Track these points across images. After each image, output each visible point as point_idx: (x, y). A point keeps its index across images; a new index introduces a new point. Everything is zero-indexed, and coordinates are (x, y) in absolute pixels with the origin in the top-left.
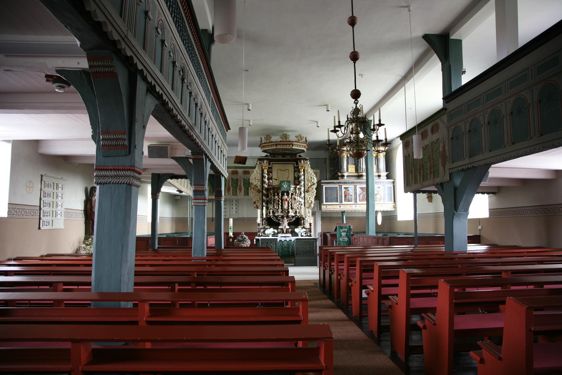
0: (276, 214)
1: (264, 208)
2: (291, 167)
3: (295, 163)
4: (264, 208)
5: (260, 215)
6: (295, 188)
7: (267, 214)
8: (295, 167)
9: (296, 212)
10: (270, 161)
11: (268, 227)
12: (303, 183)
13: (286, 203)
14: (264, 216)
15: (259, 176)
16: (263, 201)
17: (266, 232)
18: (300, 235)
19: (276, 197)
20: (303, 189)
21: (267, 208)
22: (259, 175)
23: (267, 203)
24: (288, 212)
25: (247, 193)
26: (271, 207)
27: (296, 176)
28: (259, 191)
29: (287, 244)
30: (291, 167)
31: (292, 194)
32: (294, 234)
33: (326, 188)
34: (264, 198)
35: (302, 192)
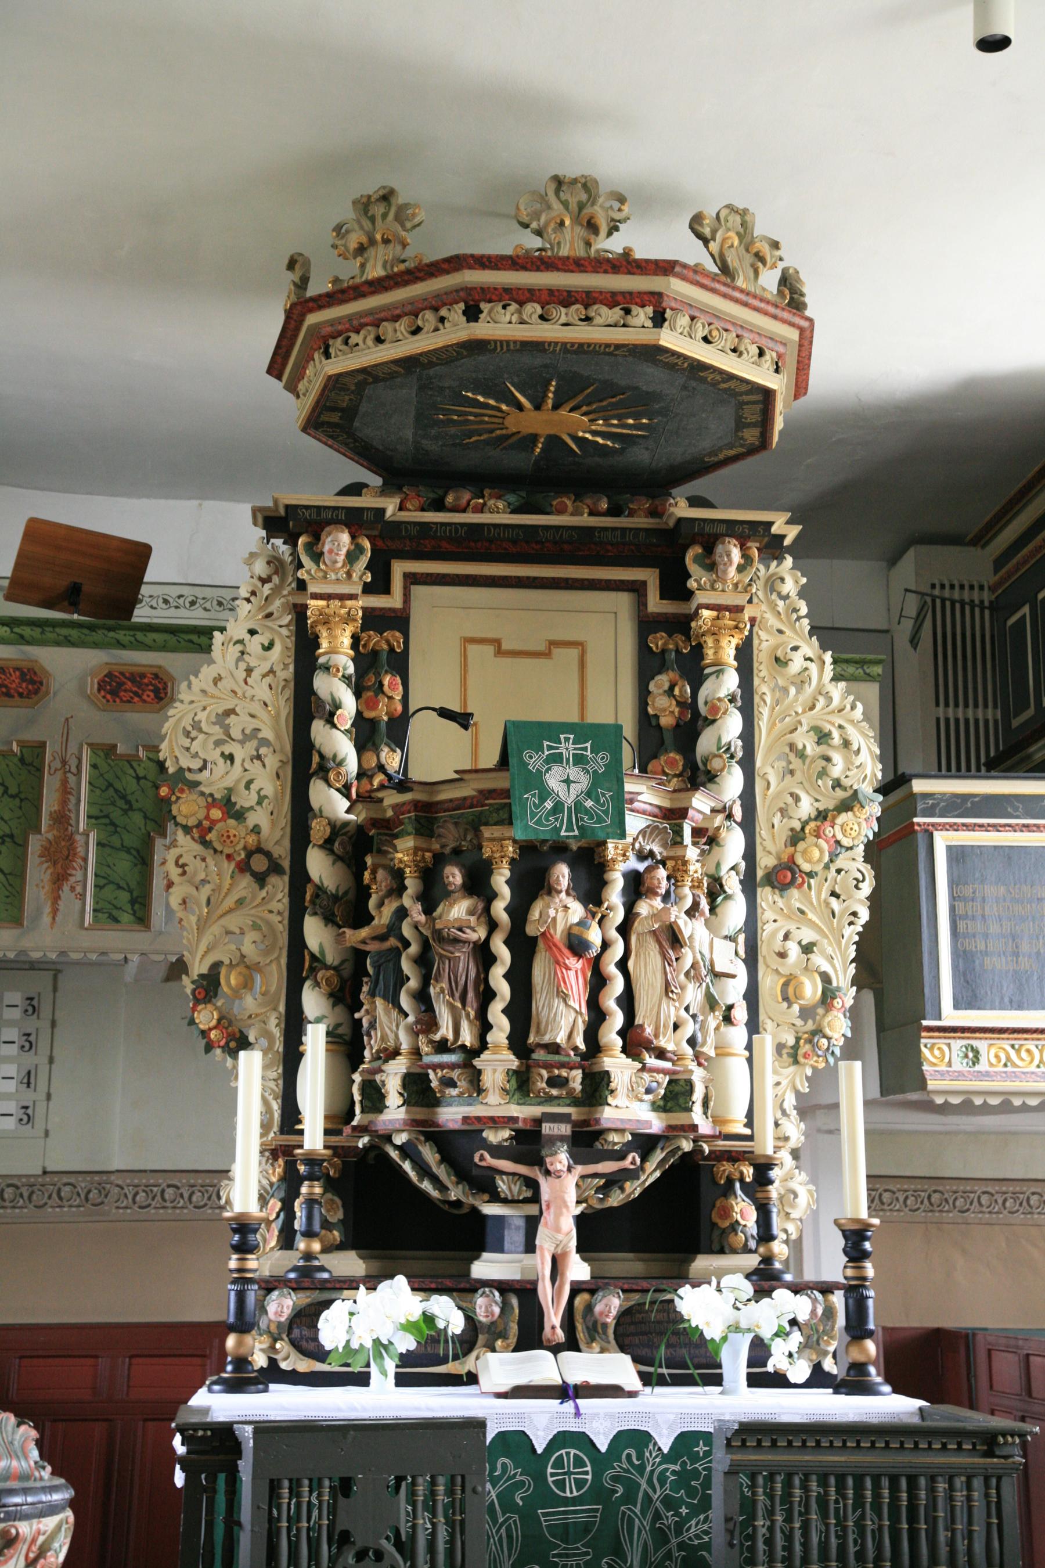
0: (451, 1115)
1: (315, 1041)
2: (603, 625)
3: (650, 576)
4: (315, 1041)
5: (248, 1124)
6: (674, 815)
7: (339, 1119)
8: (646, 625)
9: (676, 1096)
10: (387, 546)
11: (349, 1264)
12: (733, 783)
13: (575, 977)
14: (313, 1137)
15: (265, 707)
16: (299, 965)
17: (333, 1328)
18: (735, 1363)
19: (458, 910)
20: (734, 843)
21: (348, 1047)
22: (261, 689)
23: (346, 996)
24: (597, 1087)
25: (131, 899)
26: (389, 1024)
27: (665, 709)
28: (256, 865)
29: (598, 1493)
30: (603, 625)
31: (637, 887)
32: (678, 1357)
33: (956, 854)
34: (316, 934)
35: (733, 884)
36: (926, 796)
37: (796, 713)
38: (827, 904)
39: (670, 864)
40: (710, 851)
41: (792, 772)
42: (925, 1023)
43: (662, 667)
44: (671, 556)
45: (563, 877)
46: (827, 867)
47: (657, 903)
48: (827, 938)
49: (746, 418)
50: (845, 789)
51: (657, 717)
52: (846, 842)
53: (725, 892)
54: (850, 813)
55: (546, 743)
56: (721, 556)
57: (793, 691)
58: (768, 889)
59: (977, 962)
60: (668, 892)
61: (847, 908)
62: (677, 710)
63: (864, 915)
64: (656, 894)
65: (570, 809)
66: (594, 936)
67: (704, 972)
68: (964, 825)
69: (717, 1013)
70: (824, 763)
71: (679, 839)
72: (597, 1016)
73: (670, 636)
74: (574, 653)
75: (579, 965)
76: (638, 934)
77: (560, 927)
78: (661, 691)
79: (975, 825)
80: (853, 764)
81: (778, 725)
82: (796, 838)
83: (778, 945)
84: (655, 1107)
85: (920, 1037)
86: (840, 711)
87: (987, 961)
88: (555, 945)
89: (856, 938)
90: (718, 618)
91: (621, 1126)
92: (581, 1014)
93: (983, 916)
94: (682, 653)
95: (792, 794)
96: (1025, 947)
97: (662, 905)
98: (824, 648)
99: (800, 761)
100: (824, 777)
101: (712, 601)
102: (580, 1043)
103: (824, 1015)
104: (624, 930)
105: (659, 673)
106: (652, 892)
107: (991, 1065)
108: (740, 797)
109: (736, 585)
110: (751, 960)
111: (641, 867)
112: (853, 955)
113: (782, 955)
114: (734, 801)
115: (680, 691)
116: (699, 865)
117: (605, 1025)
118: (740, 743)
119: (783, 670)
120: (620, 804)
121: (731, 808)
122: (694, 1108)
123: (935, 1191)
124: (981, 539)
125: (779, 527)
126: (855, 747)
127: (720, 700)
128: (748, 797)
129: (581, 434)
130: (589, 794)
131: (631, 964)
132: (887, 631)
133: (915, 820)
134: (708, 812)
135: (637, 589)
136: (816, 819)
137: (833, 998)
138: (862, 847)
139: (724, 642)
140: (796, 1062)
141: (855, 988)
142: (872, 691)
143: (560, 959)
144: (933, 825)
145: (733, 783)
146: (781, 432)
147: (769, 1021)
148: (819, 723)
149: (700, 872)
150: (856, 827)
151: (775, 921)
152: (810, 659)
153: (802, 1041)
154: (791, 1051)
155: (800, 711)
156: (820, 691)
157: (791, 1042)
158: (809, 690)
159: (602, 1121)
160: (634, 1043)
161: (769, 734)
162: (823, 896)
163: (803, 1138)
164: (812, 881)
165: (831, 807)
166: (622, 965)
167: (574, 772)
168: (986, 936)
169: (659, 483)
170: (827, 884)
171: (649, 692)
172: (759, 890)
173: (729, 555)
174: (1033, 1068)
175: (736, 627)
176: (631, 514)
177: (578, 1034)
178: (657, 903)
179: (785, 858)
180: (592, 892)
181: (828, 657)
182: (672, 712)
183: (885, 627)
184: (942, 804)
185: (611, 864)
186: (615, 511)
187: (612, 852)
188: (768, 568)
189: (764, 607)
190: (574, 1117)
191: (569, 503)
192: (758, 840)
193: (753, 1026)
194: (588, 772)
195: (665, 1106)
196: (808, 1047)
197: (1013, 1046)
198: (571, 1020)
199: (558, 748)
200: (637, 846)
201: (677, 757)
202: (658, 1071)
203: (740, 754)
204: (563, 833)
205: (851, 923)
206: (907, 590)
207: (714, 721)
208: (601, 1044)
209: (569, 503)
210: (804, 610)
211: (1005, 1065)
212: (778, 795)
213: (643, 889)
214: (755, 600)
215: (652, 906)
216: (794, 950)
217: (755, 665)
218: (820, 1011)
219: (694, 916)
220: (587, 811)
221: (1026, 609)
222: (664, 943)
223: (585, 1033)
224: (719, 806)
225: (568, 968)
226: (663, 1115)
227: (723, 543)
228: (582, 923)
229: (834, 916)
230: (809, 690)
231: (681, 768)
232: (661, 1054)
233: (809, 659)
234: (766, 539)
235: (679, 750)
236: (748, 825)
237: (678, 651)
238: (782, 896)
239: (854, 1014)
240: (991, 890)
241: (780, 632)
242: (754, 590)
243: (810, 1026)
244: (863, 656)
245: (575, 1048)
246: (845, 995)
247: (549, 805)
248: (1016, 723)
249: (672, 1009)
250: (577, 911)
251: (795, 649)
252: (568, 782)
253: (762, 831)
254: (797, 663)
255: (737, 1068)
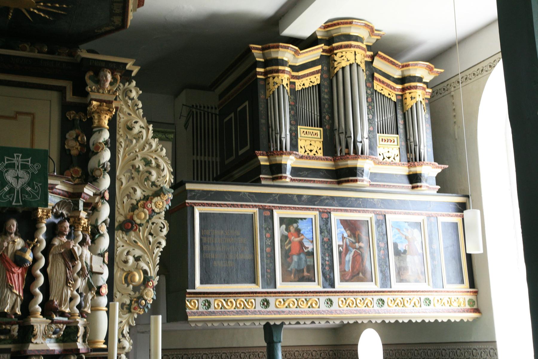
6: (73, 197)
8: (65, 107)
9: (69, 334)
12: (106, 182)
20: (105, 211)
24: (27, 333)
27: (73, 146)
33: (203, 216)
35: (103, 229)
36: (191, 191)
37: (136, 151)
38: (147, 238)
39: (72, 220)
40: (93, 213)
41: (133, 178)
42: (188, 291)
43: (73, 127)
44: (79, 77)
45: (13, 226)
46: (148, 222)
47: (64, 239)
48: (146, 253)
49: (115, 11)
50: (156, 186)
51: (69, 150)
52: (157, 210)
53: (99, 233)
54: (159, 198)
55: (6, 158)
56: (102, 77)
57: (134, 141)
58: (120, 232)
59: (211, 263)
60: (70, 233)
61: (156, 240)
62: (79, 148)
63: (164, 244)
64: (64, 235)
65: (18, 192)
66: (29, 256)
67: (87, 272)
68: (207, 204)
69: (92, 292)
70: (147, 174)
71: (76, 208)
72: (29, 296)
73: (77, 113)
74: (29, 118)
75: (20, 271)
76: (53, 255)
77: (10, 251)
78: (72, 138)
79: (212, 204)
80: (161, 175)
81: (127, 156)
82: (134, 208)
83: (124, 258)
84: (58, 341)
85: (185, 297)
86: (156, 151)
87: (215, 263)
88: (6, 261)
89: (160, 254)
90: (100, 105)
91: (37, 353)
92: (20, 296)
93: (214, 244)
94: (82, 121)
95: (132, 188)
96: (231, 257)
97: (67, 240)
98: (149, 122)
99: (137, 173)
100: (148, 181)
101: (97, 98)
102: (18, 311)
103: (144, 289)
104: (46, 253)
105: (71, 129)
106: (62, 234)
107: (215, 308)
108: (108, 189)
109: (109, 91)
110: (111, 266)
111: (57, 221)
112: (158, 261)
113: (126, 262)
114: (105, 191)
115: (81, 139)
116: (86, 220)
117: (33, 301)
118: (109, 164)
119: (130, 132)
120: (46, 189)
121: (104, 194)
122: (78, 340)
123: (185, 354)
124: (212, 87)
125: (130, 67)
126: (162, 168)
127: (100, 143)
128: (112, 188)
129: (32, 10)
130: (29, 184)
131: (48, 269)
132: (173, 124)
133: (187, 201)
134: (92, 195)
135: (62, 90)
136: (143, 199)
137: (149, 281)
138: (164, 213)
139: (103, 117)
140: (130, 311)
141: (158, 277)
142: (170, 144)
143: (9, 268)
144: (194, 203)
145: (106, 182)
146: (131, 21)
147: (118, 293)
148: (146, 156)
149: (87, 224)
150: (161, 204)
151: (123, 246)
152: (143, 128)
153: (133, 302)
154: (128, 307)
155: (138, 151)
156: (147, 142)
157: (128, 302)
158: (142, 142)
159: (27, 352)
160: (48, 310)
161: (123, 160)
162: (145, 235)
163: (131, 347)
164: (141, 228)
165: (150, 194)
166: (44, 270)
167: (21, 173)
168: (215, 252)
169: (75, 40)
170: (147, 230)
171: (66, 139)
172: (116, 232)
173: (106, 77)
174: (232, 309)
175: (109, 110)
176: (59, 54)
177: (17, 306)
178: (64, 239)
179: (129, 217)
180: (29, 233)
181: (151, 127)
182: (77, 148)
183: (172, 122)
184: (198, 195)
185: (40, 220)
186: (51, 52)
187: (41, 213)
188: (124, 85)
189: (122, 103)
190: (12, 350)
191: (28, 47)
192: (116, 209)
193: (111, 297)
194: (29, 173)
195: (63, 339)
196: (136, 304)
197: (224, 300)
198: (14, 299)
199: (12, 160)
200: (55, 210)
201: (79, 169)
202: (60, 322)
203: (109, 169)
204: (14, 204)
205: (158, 247)
206: (183, 105)
207: (97, 153)
208: (30, 311)
209: (28, 47)
210: (140, 105)
211: (221, 308)
212: (126, 188)
213: (57, 232)
214: (118, 99)
215: (61, 241)
216: (131, 259)
217: (117, 129)
218: (142, 288)
219: (83, 245)
220: (27, 193)
221: (247, 103)
222: (66, 259)
223: (21, 306)
224: (98, 192)
225: (13, 273)
226: (62, 344)
227: (103, 71)
228: (23, 250)
229: (150, 244)
230: (142, 142)
231: (80, 174)
232: (63, 314)
233: (140, 125)
234: (124, 71)
235: (79, 166)
236: (112, 202)
237: (81, 120)
238: (126, 235)
239: (157, 289)
240: (217, 232)
241: (129, 114)
242: (118, 94)
243: (137, 294)
244: (165, 130)
245: (16, 314)
246: (154, 280)
247: (6, 189)
248: (227, 162)
249: (69, 292)
250: (20, 243)
251: (136, 122)
252: (17, 178)
253: (119, 205)
254: (137, 129)
255: (103, 317)
